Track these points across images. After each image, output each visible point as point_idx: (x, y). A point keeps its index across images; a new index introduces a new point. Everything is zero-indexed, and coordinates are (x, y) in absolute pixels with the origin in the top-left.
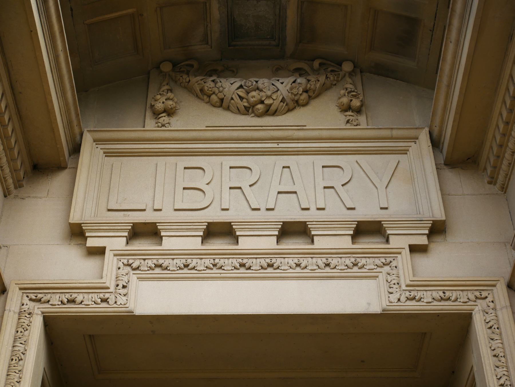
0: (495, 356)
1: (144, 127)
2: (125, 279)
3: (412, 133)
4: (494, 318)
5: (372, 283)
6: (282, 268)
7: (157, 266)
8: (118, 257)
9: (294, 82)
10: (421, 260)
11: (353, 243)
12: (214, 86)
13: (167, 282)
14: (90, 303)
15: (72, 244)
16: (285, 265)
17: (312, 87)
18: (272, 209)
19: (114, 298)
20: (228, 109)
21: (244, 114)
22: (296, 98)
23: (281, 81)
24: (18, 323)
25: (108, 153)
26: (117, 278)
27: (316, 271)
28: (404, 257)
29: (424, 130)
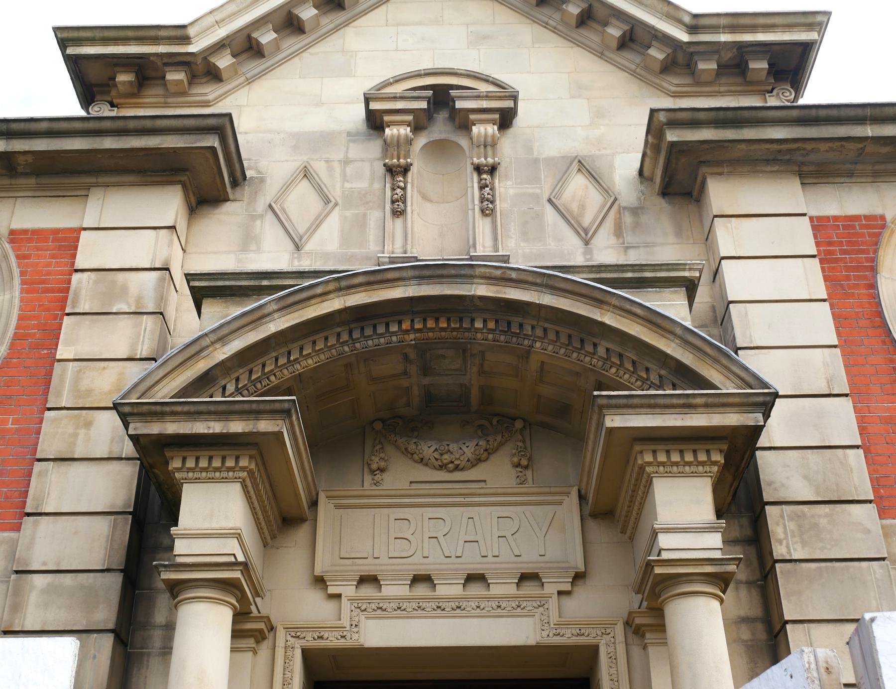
0: (611, 680)
1: (363, 487)
2: (357, 619)
3: (566, 490)
4: (614, 650)
5: (530, 620)
6: (467, 609)
7: (378, 608)
8: (351, 601)
9: (477, 445)
10: (567, 602)
11: (518, 590)
12: (415, 448)
13: (386, 620)
14: (333, 639)
15: (317, 588)
16: (469, 607)
17: (491, 447)
18: (460, 557)
19: (350, 635)
20: (427, 465)
21: (439, 470)
22: (479, 457)
23: (467, 445)
24: (285, 656)
25: (337, 506)
26: (351, 618)
27: (491, 612)
28: (554, 601)
29: (575, 488)
